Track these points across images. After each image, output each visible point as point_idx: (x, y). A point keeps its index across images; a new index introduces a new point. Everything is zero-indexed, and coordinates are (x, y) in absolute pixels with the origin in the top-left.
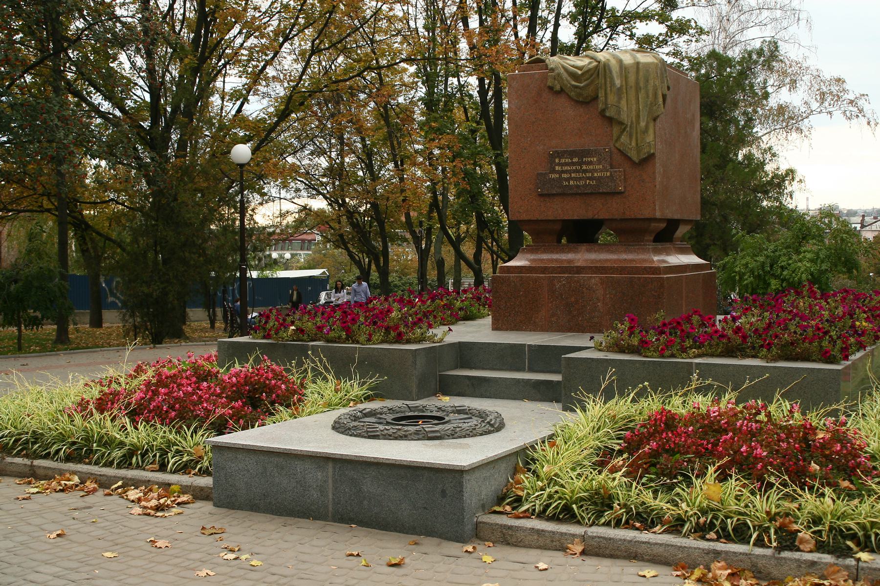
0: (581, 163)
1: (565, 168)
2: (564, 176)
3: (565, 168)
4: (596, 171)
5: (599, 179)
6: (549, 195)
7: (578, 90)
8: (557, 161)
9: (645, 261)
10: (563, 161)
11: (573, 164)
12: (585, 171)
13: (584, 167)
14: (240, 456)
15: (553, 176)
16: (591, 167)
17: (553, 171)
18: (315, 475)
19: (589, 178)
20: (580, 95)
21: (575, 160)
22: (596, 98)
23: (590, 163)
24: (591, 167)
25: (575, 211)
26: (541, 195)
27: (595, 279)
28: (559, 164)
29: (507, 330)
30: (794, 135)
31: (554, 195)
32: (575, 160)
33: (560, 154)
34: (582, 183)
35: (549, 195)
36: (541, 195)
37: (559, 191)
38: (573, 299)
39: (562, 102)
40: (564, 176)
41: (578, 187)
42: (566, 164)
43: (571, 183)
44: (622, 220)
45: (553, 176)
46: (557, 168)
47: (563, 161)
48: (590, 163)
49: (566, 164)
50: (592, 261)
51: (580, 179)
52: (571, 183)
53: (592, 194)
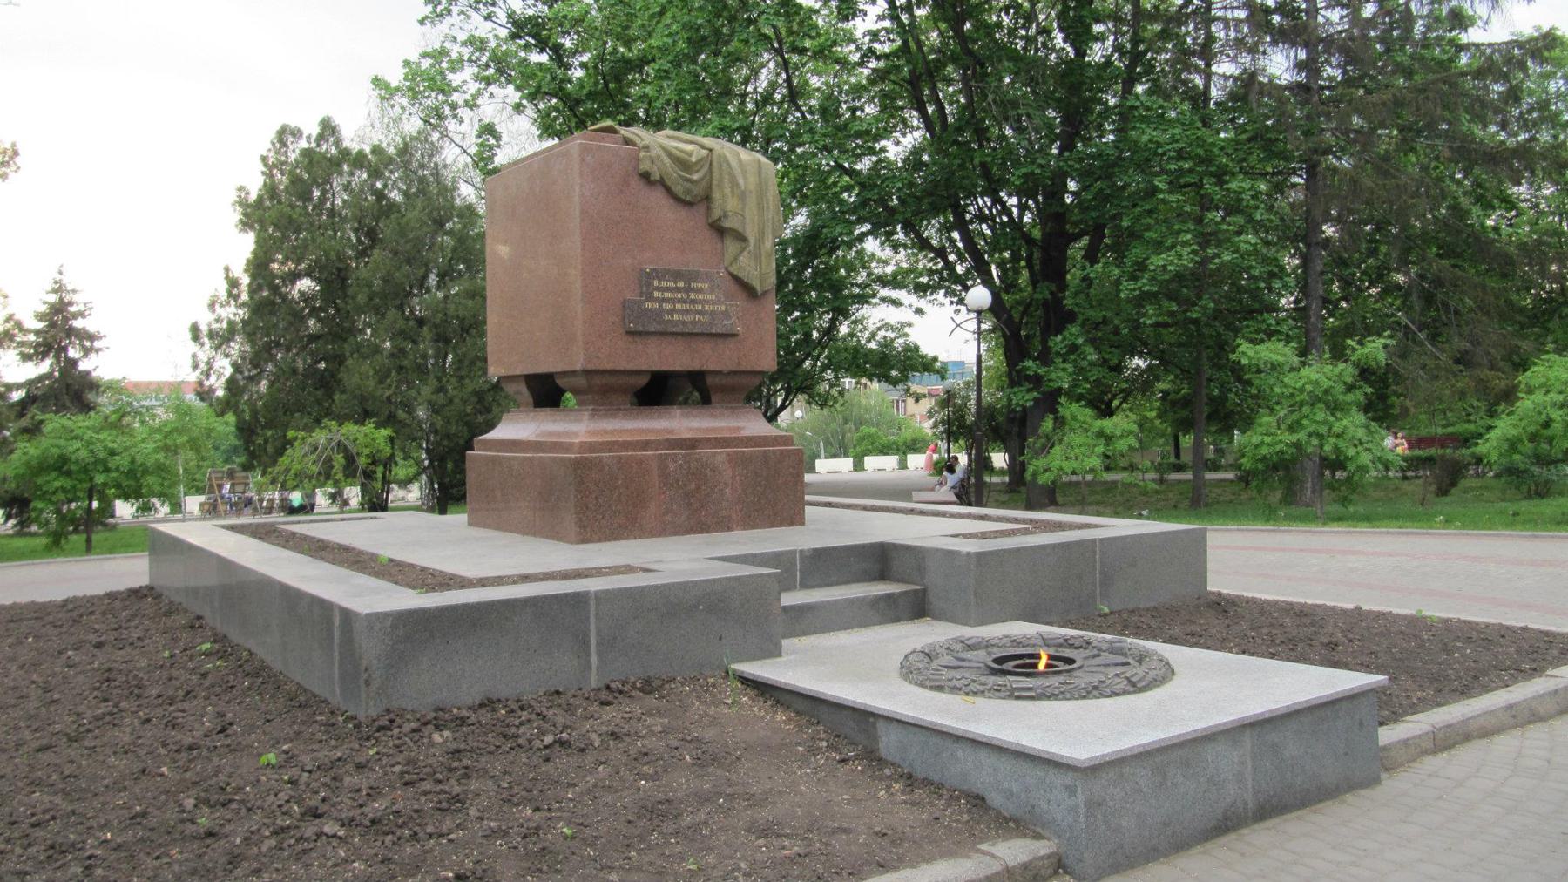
0: (688, 290)
1: (668, 295)
2: (667, 306)
3: (668, 295)
4: (707, 302)
5: (712, 313)
6: (640, 334)
7: (688, 185)
8: (656, 283)
9: (738, 429)
10: (664, 284)
11: (677, 290)
12: (693, 302)
13: (692, 296)
14: (1126, 770)
15: (650, 305)
16: (701, 297)
17: (651, 298)
18: (1228, 760)
19: (700, 313)
20: (688, 191)
21: (681, 284)
22: (707, 198)
23: (700, 291)
24: (701, 297)
25: (674, 358)
26: (630, 333)
27: (720, 456)
28: (659, 289)
29: (600, 541)
30: (43, 308)
31: (648, 334)
32: (681, 284)
33: (661, 274)
34: (689, 318)
35: (640, 334)
36: (630, 333)
37: (660, 328)
38: (693, 486)
39: (657, 197)
40: (667, 306)
41: (684, 323)
42: (669, 289)
43: (676, 317)
44: (735, 373)
45: (650, 305)
46: (656, 294)
47: (664, 284)
48: (700, 291)
49: (669, 289)
50: (708, 430)
51: (687, 312)
52: (676, 317)
53: (701, 334)
